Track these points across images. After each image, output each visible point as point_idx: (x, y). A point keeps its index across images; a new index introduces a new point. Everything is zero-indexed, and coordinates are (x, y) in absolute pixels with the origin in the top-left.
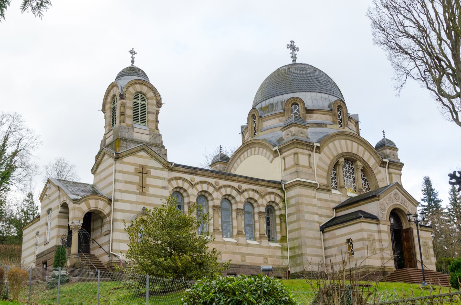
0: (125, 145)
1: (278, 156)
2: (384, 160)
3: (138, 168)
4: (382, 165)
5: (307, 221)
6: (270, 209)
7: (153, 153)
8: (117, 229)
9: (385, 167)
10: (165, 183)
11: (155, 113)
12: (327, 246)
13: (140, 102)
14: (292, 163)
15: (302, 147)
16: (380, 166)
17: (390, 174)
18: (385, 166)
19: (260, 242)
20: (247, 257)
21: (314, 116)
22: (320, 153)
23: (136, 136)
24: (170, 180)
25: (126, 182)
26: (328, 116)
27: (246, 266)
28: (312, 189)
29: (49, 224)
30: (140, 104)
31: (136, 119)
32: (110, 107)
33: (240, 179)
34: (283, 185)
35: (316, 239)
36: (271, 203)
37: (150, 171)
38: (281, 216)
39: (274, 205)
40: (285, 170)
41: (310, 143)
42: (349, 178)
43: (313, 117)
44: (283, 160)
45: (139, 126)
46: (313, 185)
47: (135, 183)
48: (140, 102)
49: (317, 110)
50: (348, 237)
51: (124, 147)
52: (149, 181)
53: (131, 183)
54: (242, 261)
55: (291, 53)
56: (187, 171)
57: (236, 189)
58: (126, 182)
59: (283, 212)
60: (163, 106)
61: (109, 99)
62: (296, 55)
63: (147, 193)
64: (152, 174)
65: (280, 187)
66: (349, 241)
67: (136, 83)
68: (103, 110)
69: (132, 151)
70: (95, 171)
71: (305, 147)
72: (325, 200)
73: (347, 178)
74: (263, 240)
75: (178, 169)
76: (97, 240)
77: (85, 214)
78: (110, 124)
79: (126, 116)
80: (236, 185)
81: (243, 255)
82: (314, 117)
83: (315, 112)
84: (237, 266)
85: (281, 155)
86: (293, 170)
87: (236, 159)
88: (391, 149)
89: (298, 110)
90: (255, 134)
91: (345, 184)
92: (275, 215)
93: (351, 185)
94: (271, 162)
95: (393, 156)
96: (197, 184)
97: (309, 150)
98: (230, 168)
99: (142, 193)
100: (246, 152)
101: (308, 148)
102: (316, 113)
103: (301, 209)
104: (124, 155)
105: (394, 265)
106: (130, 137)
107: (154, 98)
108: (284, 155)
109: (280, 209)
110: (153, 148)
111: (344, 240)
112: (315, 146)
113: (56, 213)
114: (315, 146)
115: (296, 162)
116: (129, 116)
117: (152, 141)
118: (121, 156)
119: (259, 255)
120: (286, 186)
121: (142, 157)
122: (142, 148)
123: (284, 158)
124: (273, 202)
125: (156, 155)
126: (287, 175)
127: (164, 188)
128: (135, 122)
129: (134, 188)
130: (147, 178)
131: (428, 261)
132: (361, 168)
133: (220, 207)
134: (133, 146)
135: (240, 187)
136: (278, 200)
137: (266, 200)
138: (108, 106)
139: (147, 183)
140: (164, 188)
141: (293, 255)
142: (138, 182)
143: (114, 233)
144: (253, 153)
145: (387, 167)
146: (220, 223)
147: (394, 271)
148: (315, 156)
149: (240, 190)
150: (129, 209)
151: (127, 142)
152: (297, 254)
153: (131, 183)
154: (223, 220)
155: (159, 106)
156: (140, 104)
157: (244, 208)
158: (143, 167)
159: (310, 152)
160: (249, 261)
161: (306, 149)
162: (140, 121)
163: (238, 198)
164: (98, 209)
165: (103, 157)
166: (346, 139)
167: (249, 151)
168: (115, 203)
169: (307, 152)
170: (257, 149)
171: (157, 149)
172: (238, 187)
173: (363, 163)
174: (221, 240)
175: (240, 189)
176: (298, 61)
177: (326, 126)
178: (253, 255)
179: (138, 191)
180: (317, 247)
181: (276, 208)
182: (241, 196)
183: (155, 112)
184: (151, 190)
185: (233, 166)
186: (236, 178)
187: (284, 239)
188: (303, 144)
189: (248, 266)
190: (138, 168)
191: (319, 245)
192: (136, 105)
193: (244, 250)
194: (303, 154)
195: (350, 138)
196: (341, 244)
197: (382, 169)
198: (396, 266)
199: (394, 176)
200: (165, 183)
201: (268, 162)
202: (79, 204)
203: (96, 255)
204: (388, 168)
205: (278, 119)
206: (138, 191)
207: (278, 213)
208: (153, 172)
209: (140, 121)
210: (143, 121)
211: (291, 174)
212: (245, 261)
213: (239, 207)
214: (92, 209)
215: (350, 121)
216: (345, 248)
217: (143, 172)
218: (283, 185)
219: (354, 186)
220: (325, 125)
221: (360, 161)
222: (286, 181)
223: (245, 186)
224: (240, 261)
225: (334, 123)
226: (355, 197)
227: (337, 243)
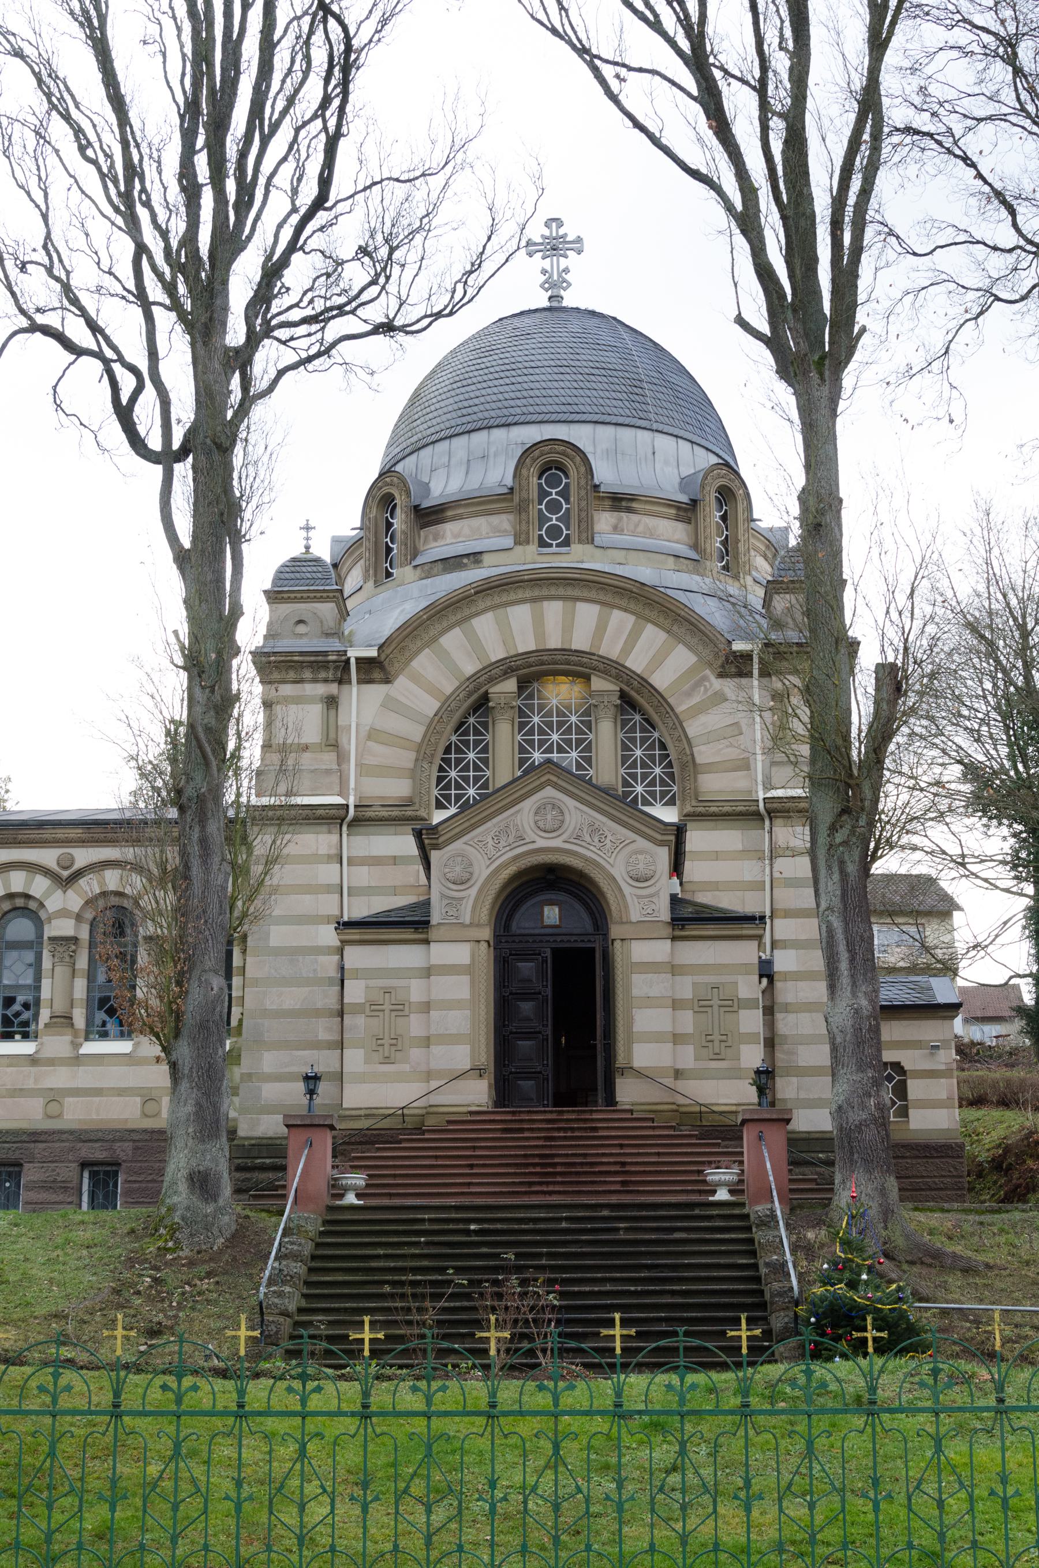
5: (278, 952)
15: (292, 675)
16: (721, 675)
20: (69, 1101)
21: (449, 529)
22: (387, 681)
26: (504, 517)
27: (61, 1132)
28: (325, 828)
33: (61, 833)
35: (317, 1013)
43: (443, 537)
46: (320, 812)
49: (456, 503)
55: (544, 272)
57: (46, 872)
62: (566, 270)
71: (307, 674)
72: (395, 860)
80: (48, 857)
81: (54, 1097)
82: (448, 534)
83: (450, 513)
84: (24, 1138)
89: (565, 494)
97: (326, 681)
101: (323, 675)
102: (454, 518)
112: (353, 661)
114: (353, 661)
119: (121, 1092)
131: (714, 1064)
133: (91, 925)
143: (776, 921)
145: (756, 672)
146: (46, 983)
148: (361, 703)
159: (333, 688)
160: (76, 1114)
161: (315, 681)
163: (55, 901)
166: (534, 600)
168: (353, 868)
169: (321, 689)
173: (617, 677)
176: (570, 300)
178: (98, 1092)
180: (316, 1045)
182: (70, 892)
186: (47, 834)
188: (299, 666)
189: (71, 1132)
191: (323, 1035)
193: (59, 1078)
194: (298, 700)
195: (561, 592)
197: (728, 686)
204: (764, 674)
212: (59, 1116)
221: (492, 680)
223: (83, 856)
225: (521, 539)
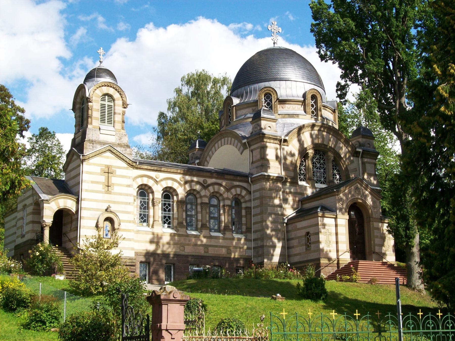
0: (91, 147)
1: (247, 148)
2: (358, 150)
3: (104, 168)
4: (355, 155)
6: (237, 201)
7: (118, 154)
8: (84, 226)
9: (358, 157)
10: (130, 182)
11: (122, 114)
12: (290, 237)
13: (107, 103)
14: (258, 157)
17: (363, 163)
18: (358, 155)
19: (224, 234)
20: (210, 248)
23: (103, 138)
24: (135, 179)
25: (92, 182)
27: (208, 257)
29: (25, 218)
30: (106, 106)
31: (103, 120)
32: (80, 108)
34: (250, 178)
36: (237, 196)
37: (115, 170)
38: (246, 208)
39: (240, 198)
40: (252, 163)
41: (277, 136)
42: (320, 169)
44: (251, 152)
45: (106, 127)
47: (100, 182)
48: (107, 103)
50: (307, 230)
51: (90, 149)
52: (114, 180)
53: (97, 183)
54: (205, 252)
56: (152, 168)
58: (92, 182)
59: (248, 205)
60: (128, 106)
61: (79, 100)
63: (112, 191)
64: (117, 174)
65: (247, 179)
66: (308, 233)
67: (103, 86)
68: (74, 109)
69: (98, 153)
70: (66, 169)
73: (317, 169)
74: (227, 233)
75: (143, 167)
76: (67, 235)
77: (59, 208)
78: (79, 125)
79: (93, 118)
85: (249, 147)
86: (259, 164)
87: (211, 147)
88: (367, 138)
90: (230, 123)
91: (314, 175)
92: (241, 207)
93: (321, 176)
94: (241, 154)
95: (368, 145)
96: (162, 180)
98: (206, 155)
99: (108, 192)
100: (217, 144)
103: (264, 202)
104: (90, 156)
105: (349, 257)
106: (96, 139)
107: (121, 99)
108: (252, 147)
109: (245, 202)
110: (119, 149)
111: (303, 233)
113: (30, 209)
115: (262, 156)
116: (96, 119)
117: (118, 142)
118: (87, 158)
120: (253, 179)
121: (107, 157)
122: (107, 149)
123: (252, 151)
124: (239, 195)
125: (121, 156)
126: (254, 168)
127: (129, 186)
128: (102, 123)
129: (100, 187)
130: (112, 177)
132: (332, 158)
134: (99, 147)
135: (205, 181)
136: (244, 193)
137: (232, 194)
138: (78, 106)
139: (112, 182)
140: (129, 186)
141: (257, 246)
142: (104, 181)
144: (223, 144)
147: (349, 263)
149: (205, 185)
150: (95, 207)
151: (93, 144)
152: (259, 245)
153: (97, 183)
154: (188, 213)
155: (125, 106)
156: (106, 106)
157: (209, 201)
158: (108, 167)
162: (106, 122)
164: (67, 208)
165: (73, 156)
167: (223, 140)
170: (230, 139)
171: (122, 149)
172: (203, 182)
174: (184, 233)
175: (205, 184)
177: (298, 117)
179: (104, 190)
181: (242, 200)
182: (206, 190)
183: (121, 112)
184: (116, 189)
185: (208, 153)
187: (249, 230)
189: (211, 257)
190: (104, 168)
192: (103, 106)
196: (301, 237)
198: (351, 257)
199: (367, 165)
200: (130, 182)
201: (238, 153)
202: (49, 203)
203: (67, 248)
205: (251, 108)
206: (104, 190)
207: (244, 205)
208: (119, 172)
209: (106, 122)
210: (110, 122)
211: (257, 167)
212: (208, 252)
213: (203, 201)
214: (61, 207)
215: (326, 110)
216: (304, 241)
217: (108, 172)
218: (250, 178)
219: (324, 176)
220: (297, 115)
222: (252, 175)
224: (203, 252)
226: (325, 188)
227: (299, 235)
